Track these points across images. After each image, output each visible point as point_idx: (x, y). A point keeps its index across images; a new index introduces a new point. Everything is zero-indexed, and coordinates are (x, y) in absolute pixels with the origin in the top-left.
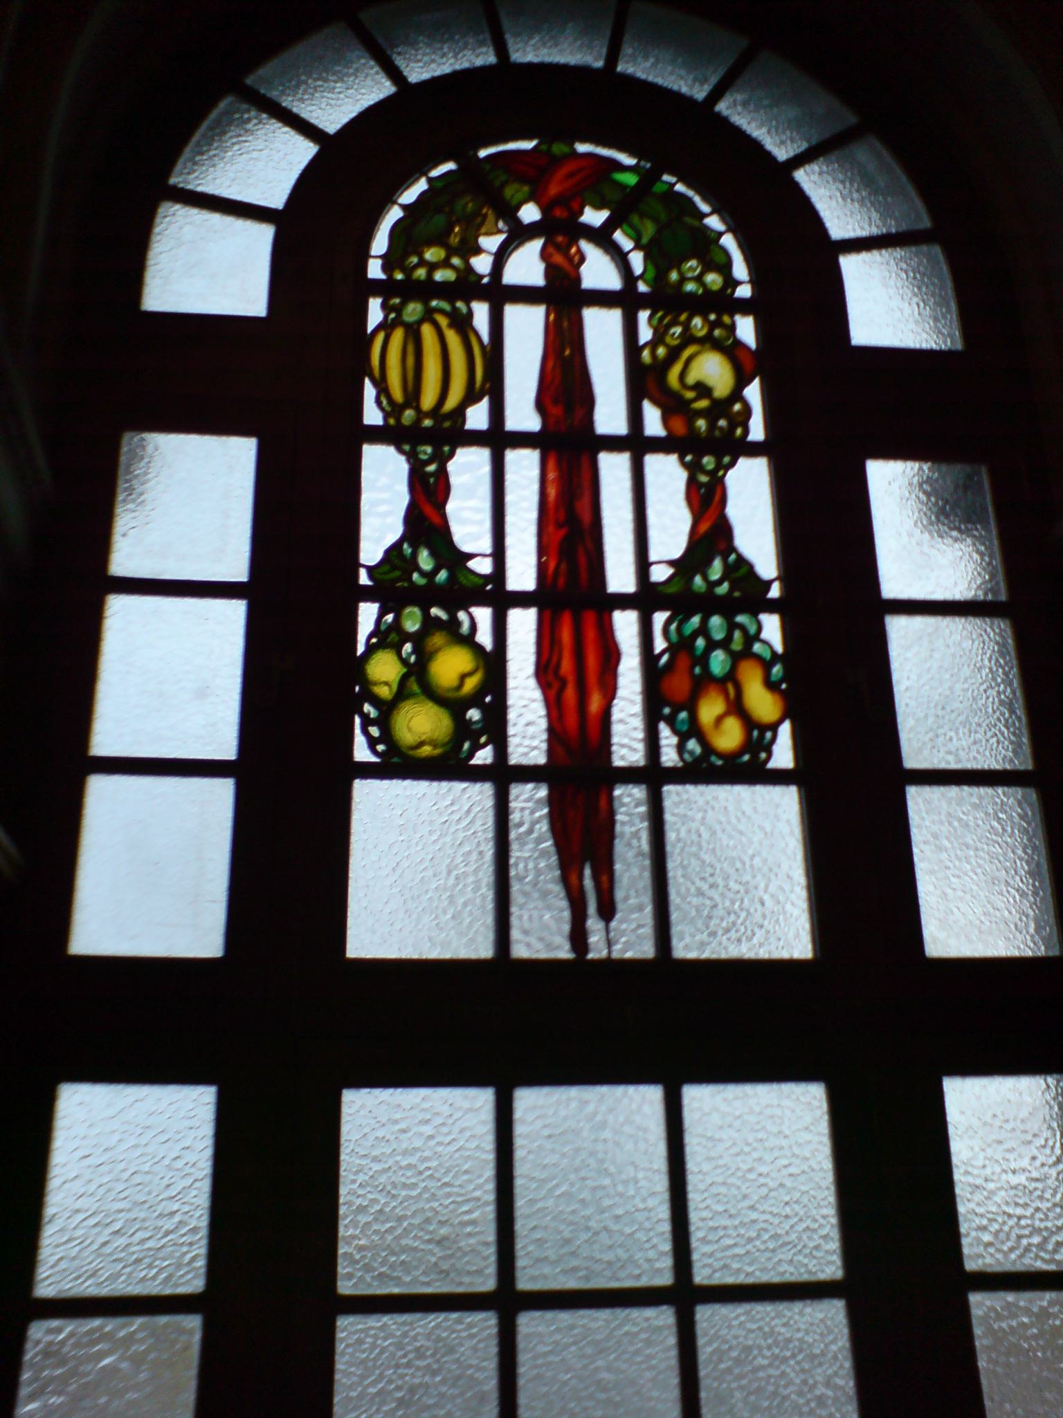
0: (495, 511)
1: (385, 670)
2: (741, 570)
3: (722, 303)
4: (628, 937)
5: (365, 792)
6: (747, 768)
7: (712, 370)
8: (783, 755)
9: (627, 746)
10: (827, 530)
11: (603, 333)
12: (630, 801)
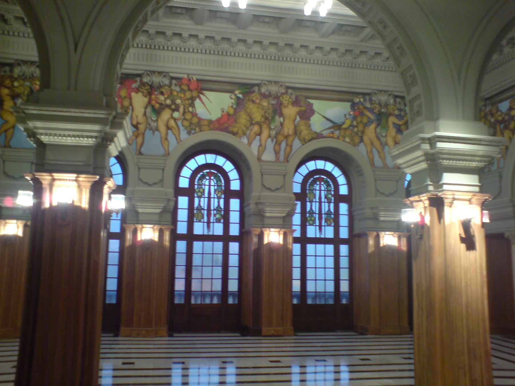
0: (315, 207)
1: (309, 219)
2: (331, 212)
3: (331, 191)
4: (323, 236)
5: (195, 223)
6: (220, 222)
7: (330, 196)
8: (333, 225)
9: (323, 224)
10: (337, 208)
11: (323, 192)
12: (323, 227)
